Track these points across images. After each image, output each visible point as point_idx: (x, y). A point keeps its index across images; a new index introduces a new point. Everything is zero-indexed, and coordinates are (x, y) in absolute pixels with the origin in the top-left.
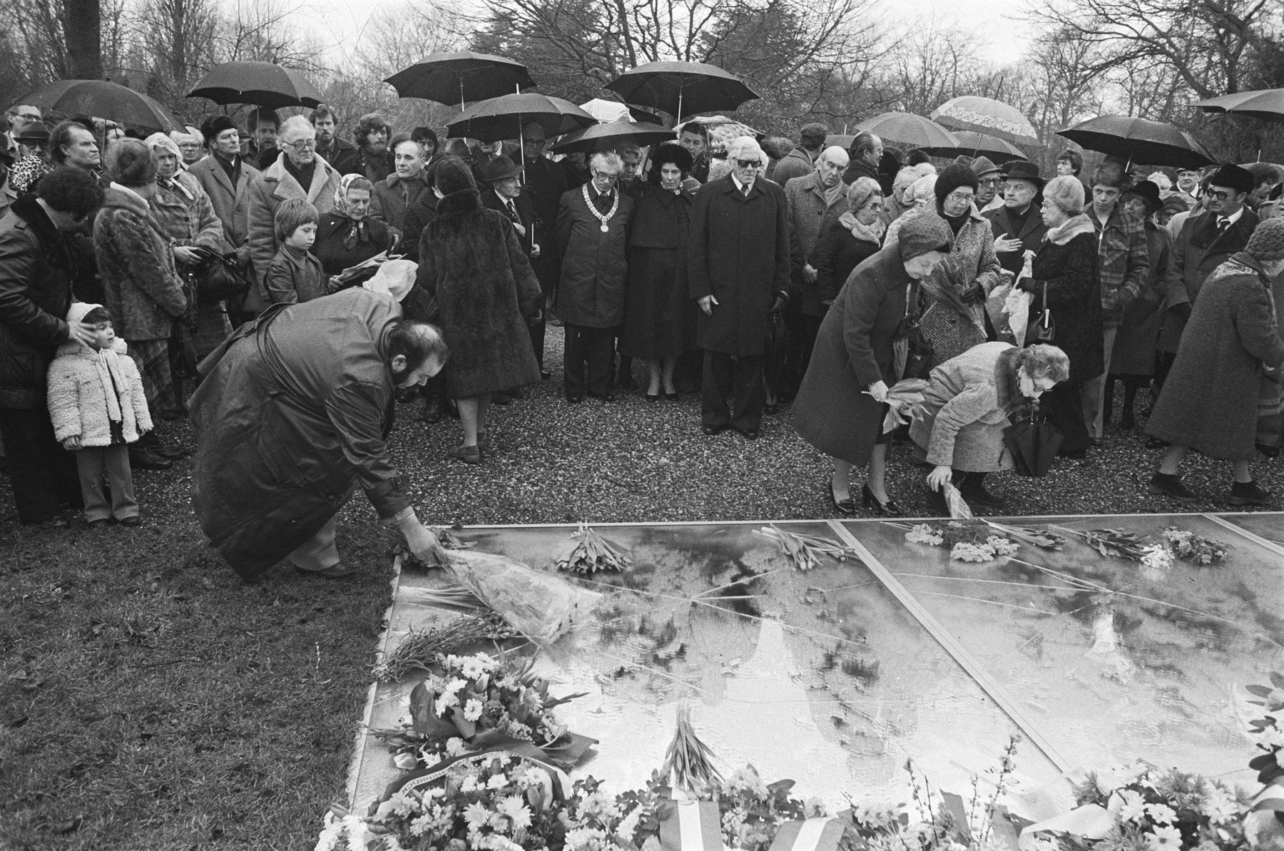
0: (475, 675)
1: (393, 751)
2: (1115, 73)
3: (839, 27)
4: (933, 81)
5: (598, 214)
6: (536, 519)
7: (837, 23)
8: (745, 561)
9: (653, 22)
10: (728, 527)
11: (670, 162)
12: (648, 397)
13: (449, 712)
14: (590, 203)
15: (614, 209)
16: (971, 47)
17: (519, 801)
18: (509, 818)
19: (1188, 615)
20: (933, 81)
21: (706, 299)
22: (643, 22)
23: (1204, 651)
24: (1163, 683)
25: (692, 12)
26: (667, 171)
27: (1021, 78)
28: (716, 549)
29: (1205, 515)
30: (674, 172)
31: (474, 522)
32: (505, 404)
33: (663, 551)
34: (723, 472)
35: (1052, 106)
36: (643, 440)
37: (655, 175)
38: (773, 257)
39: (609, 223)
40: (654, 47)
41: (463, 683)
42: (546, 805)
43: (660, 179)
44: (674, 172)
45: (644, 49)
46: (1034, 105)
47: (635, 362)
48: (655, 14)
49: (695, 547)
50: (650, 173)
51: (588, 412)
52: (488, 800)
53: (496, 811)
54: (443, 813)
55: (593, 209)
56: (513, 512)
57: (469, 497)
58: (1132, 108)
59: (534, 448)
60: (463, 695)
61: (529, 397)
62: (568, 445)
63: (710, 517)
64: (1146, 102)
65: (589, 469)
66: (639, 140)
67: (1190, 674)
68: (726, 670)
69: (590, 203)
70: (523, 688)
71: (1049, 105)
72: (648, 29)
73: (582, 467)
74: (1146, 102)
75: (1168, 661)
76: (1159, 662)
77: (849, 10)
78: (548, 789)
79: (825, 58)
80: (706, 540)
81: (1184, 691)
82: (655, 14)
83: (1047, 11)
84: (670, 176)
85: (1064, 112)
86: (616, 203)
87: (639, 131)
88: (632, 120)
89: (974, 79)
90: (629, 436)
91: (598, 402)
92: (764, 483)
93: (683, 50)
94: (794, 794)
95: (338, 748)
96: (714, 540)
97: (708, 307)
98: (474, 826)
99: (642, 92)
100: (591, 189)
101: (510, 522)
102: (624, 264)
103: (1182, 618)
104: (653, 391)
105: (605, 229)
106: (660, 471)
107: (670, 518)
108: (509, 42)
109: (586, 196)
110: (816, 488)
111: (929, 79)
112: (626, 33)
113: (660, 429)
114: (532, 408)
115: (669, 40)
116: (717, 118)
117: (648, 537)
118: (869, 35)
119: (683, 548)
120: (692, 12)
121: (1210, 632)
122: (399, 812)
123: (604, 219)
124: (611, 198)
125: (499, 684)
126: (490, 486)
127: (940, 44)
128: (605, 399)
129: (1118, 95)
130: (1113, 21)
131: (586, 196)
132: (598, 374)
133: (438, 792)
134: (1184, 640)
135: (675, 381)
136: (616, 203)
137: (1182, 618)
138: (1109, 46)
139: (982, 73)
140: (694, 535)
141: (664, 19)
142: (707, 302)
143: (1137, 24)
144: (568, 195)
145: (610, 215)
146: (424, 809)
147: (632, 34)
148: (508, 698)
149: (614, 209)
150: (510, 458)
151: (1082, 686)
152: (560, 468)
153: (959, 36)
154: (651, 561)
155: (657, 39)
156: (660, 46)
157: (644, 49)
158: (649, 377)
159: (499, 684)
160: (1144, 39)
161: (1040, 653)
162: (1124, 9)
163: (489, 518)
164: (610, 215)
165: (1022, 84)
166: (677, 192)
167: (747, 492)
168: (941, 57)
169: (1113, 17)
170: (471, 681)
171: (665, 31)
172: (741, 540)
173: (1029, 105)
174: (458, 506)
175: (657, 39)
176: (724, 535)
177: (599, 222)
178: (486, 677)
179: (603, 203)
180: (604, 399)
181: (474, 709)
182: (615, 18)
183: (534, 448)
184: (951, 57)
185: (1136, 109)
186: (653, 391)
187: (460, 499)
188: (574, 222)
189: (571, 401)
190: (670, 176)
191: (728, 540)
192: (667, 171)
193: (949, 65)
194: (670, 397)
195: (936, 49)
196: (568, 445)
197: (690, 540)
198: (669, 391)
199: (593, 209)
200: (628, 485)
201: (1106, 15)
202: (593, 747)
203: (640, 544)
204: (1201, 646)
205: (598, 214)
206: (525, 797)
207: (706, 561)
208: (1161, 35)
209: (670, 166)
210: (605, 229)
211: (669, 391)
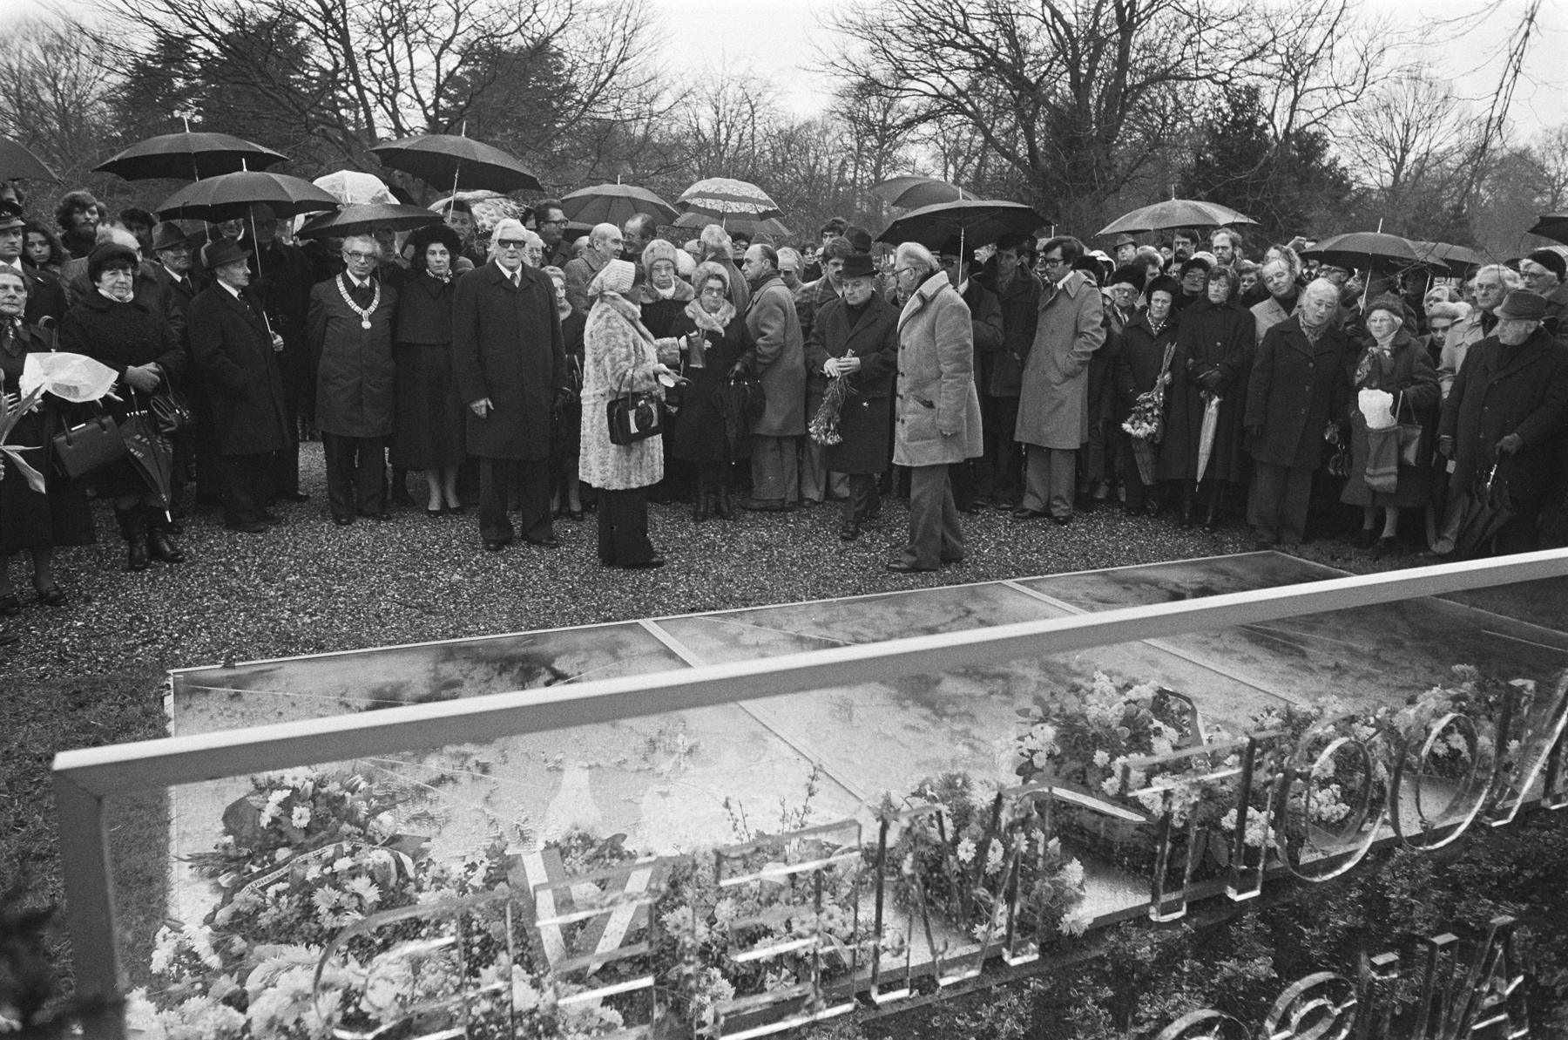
0: (298, 784)
1: (213, 875)
2: (926, 129)
3: (615, 78)
4: (728, 135)
5: (357, 309)
6: (321, 648)
7: (611, 74)
8: (557, 666)
9: (389, 70)
10: (534, 636)
11: (437, 241)
12: (429, 513)
13: (275, 820)
14: (347, 297)
15: (376, 302)
16: (768, 96)
17: (365, 880)
18: (359, 896)
19: (983, 670)
20: (728, 135)
21: (483, 402)
22: (378, 69)
23: (994, 697)
24: (958, 727)
25: (438, 58)
26: (434, 253)
27: (827, 131)
28: (526, 658)
29: (1005, 582)
30: (442, 253)
31: (248, 658)
32: (260, 531)
33: (468, 665)
34: (523, 584)
35: (863, 164)
36: (430, 558)
37: (420, 261)
38: (549, 348)
39: (370, 318)
40: (392, 99)
41: (287, 793)
42: (392, 882)
43: (425, 264)
44: (442, 253)
45: (381, 102)
46: (844, 162)
47: (410, 475)
48: (391, 60)
49: (502, 659)
50: (413, 259)
51: (361, 532)
52: (334, 880)
53: (345, 892)
54: (290, 903)
55: (351, 303)
56: (292, 645)
57: (237, 634)
58: (946, 171)
59: (305, 575)
60: (286, 805)
61: (287, 523)
62: (344, 570)
63: (515, 629)
64: (960, 160)
65: (372, 593)
66: (398, 224)
67: (982, 719)
68: (550, 764)
69: (347, 297)
70: (348, 794)
71: (859, 162)
72: (384, 79)
73: (364, 591)
74: (960, 160)
75: (962, 709)
76: (955, 710)
77: (624, 60)
78: (393, 869)
79: (605, 112)
80: (513, 651)
81: (976, 732)
82: (391, 60)
83: (844, 64)
84: (439, 257)
85: (876, 171)
86: (377, 296)
87: (400, 216)
88: (394, 201)
89: (776, 133)
90: (414, 556)
91: (370, 522)
92: (568, 592)
93: (429, 103)
94: (627, 846)
95: (150, 880)
96: (523, 651)
97: (484, 411)
98: (323, 909)
99: (392, 163)
100: (347, 281)
101: (291, 654)
102: (393, 364)
103: (977, 673)
104: (434, 506)
105: (366, 325)
106: (455, 590)
107: (470, 634)
108: (185, 78)
109: (342, 288)
110: (624, 592)
111: (724, 131)
112: (357, 83)
113: (448, 545)
114: (295, 534)
115: (410, 91)
116: (480, 193)
117: (449, 654)
118: (653, 88)
119: (489, 661)
120: (438, 58)
121: (1000, 681)
122: (243, 908)
123: (365, 314)
124: (372, 289)
125: (324, 790)
126: (260, 620)
127: (733, 92)
128: (379, 519)
129: (930, 152)
130: (912, 78)
131: (342, 288)
132: (362, 494)
133: (282, 886)
134: (979, 691)
135: (459, 494)
136: (377, 296)
137: (977, 673)
138: (910, 103)
139: (783, 125)
140: (502, 647)
141: (403, 66)
142: (481, 406)
143: (939, 82)
144: (319, 288)
145: (372, 309)
146: (268, 902)
147: (363, 82)
148: (335, 802)
149: (376, 302)
150: (278, 589)
151: (886, 738)
152: (339, 595)
153: (754, 83)
154: (457, 676)
155: (397, 90)
156: (402, 98)
157: (381, 102)
158: (429, 490)
159: (324, 790)
160: (946, 97)
161: (850, 716)
162: (922, 65)
163: (266, 653)
164: (372, 309)
165: (828, 138)
166: (447, 280)
167: (552, 602)
168: (736, 107)
169: (912, 73)
170: (295, 789)
171: (405, 81)
172: (550, 647)
173: (838, 163)
174: (225, 645)
175: (397, 90)
176: (531, 644)
177: (360, 318)
178: (310, 785)
179: (363, 296)
180: (378, 519)
181: (301, 816)
182: (342, 64)
183: (307, 575)
184: (747, 107)
185: (951, 168)
186: (434, 506)
187: (226, 637)
188: (328, 318)
189: (339, 523)
190: (439, 257)
191: (535, 649)
192: (434, 253)
193: (746, 116)
194: (455, 511)
195: (730, 98)
196: (344, 570)
197: (495, 652)
198: (453, 504)
199: (351, 303)
200: (421, 606)
201: (904, 70)
202: (425, 845)
203: (443, 661)
204: (992, 693)
205: (357, 309)
206: (372, 877)
207: (516, 671)
208: (960, 93)
209: (437, 247)
210: (366, 325)
211: (453, 504)
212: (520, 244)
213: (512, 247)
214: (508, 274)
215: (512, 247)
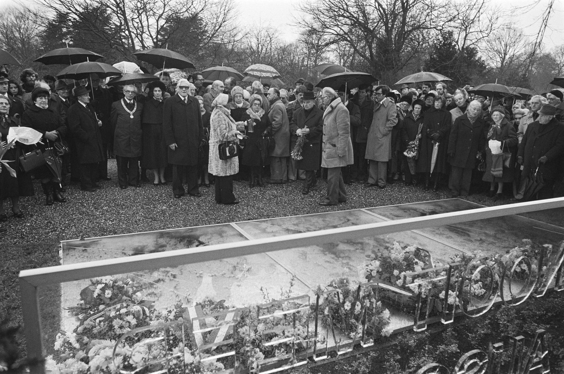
0: (107, 282)
1: (77, 315)
2: (333, 46)
3: (221, 28)
4: (262, 49)
5: (128, 111)
6: (115, 233)
7: (220, 27)
8: (200, 239)
9: (140, 25)
10: (192, 229)
11: (157, 87)
12: (154, 184)
13: (99, 295)
14: (125, 107)
15: (135, 109)
16: (276, 35)
17: (131, 317)
18: (129, 322)
19: (354, 241)
20: (262, 49)
21: (174, 145)
22: (136, 25)
23: (358, 251)
24: (345, 261)
25: (157, 21)
26: (156, 91)
27: (297, 47)
28: (189, 237)
29: (362, 209)
30: (159, 91)
31: (89, 237)
32: (93, 191)
33: (168, 239)
34: (188, 210)
35: (310, 59)
36: (155, 201)
37: (151, 94)
38: (198, 125)
39: (133, 114)
40: (141, 36)
41: (103, 285)
42: (141, 317)
43: (153, 95)
44: (159, 91)
45: (137, 37)
46: (303, 58)
47: (147, 171)
48: (141, 21)
49: (180, 237)
50: (149, 93)
51: (130, 191)
52: (120, 317)
53: (124, 321)
54: (104, 325)
55: (126, 109)
56: (105, 232)
57: (85, 228)
58: (340, 61)
59: (110, 207)
60: (103, 290)
61: (103, 188)
62: (124, 205)
63: (185, 226)
64: (345, 58)
65: (134, 213)
66: (143, 81)
67: (353, 258)
68: (198, 275)
69: (125, 107)
70: (125, 286)
71: (309, 58)
72: (138, 28)
73: (131, 213)
74: (345, 58)
75: (346, 255)
76: (343, 255)
77: (224, 21)
78: (141, 312)
79: (218, 40)
80: (184, 234)
81: (351, 263)
82: (141, 21)
83: (304, 23)
84: (158, 92)
85: (315, 61)
86: (136, 106)
87: (144, 78)
88: (142, 72)
89: (279, 48)
90: (149, 200)
91: (133, 188)
92: (204, 213)
93: (154, 37)
94: (226, 304)
95: (54, 317)
96: (188, 234)
97: (174, 148)
98: (116, 327)
99: (141, 59)
100: (125, 101)
101: (105, 235)
102: (141, 131)
103: (351, 242)
104: (156, 182)
105: (132, 117)
106: (164, 212)
107: (169, 228)
109: (123, 104)
110: (224, 213)
111: (260, 47)
112: (128, 30)
113: (161, 196)
114: (106, 192)
115: (148, 33)
116: (173, 69)
117: (162, 235)
118: (235, 32)
119: (176, 238)
120: (157, 21)
121: (360, 245)
122: (88, 327)
123: (131, 113)
124: (134, 104)
125: (117, 284)
126: (93, 223)
127: (264, 33)
128: (136, 187)
129: (335, 55)
130: (328, 28)
131: (123, 104)
132: (130, 178)
133: (101, 319)
134: (352, 249)
135: (165, 178)
136: (136, 106)
137: (351, 242)
138: (327, 37)
139: (282, 45)
140: (181, 233)
141: (145, 24)
142: (173, 146)
143: (338, 29)
144: (115, 104)
145: (134, 111)
146: (97, 324)
147: (131, 29)
148: (120, 288)
149: (135, 109)
150: (100, 212)
151: (319, 265)
152: (122, 214)
153: (271, 30)
154: (164, 243)
155: (143, 32)
156: (144, 35)
157: (137, 37)
158: (154, 176)
159: (117, 284)
160: (340, 35)
161: (306, 257)
162: (332, 23)
163: (96, 235)
164: (134, 111)
165: (298, 50)
166: (161, 101)
167: (198, 216)
168: (265, 39)
169: (328, 26)
170: (106, 284)
171: (146, 29)
172: (198, 233)
173: (301, 58)
174: (81, 232)
175: (143, 32)
176: (191, 232)
177: (129, 114)
178: (111, 282)
179: (130, 107)
180: (136, 187)
181: (108, 293)
182: (123, 23)
183: (110, 207)
184: (269, 38)
185: (342, 60)
186: (156, 182)
187: (81, 229)
188: (118, 114)
189: (122, 188)
190: (158, 92)
191: (192, 233)
192: (156, 91)
193: (268, 42)
194: (164, 184)
195: (263, 35)
196: (124, 205)
197: (178, 234)
198: (163, 181)
199: (126, 109)
200: (151, 218)
201: (325, 25)
202: (153, 304)
203: (159, 238)
204: (357, 249)
205: (128, 111)
206: (134, 315)
207: (186, 241)
208: (345, 33)
209: (157, 89)
210: (132, 117)
211: (163, 181)
212: (187, 88)
213: (184, 89)
215: (184, 89)
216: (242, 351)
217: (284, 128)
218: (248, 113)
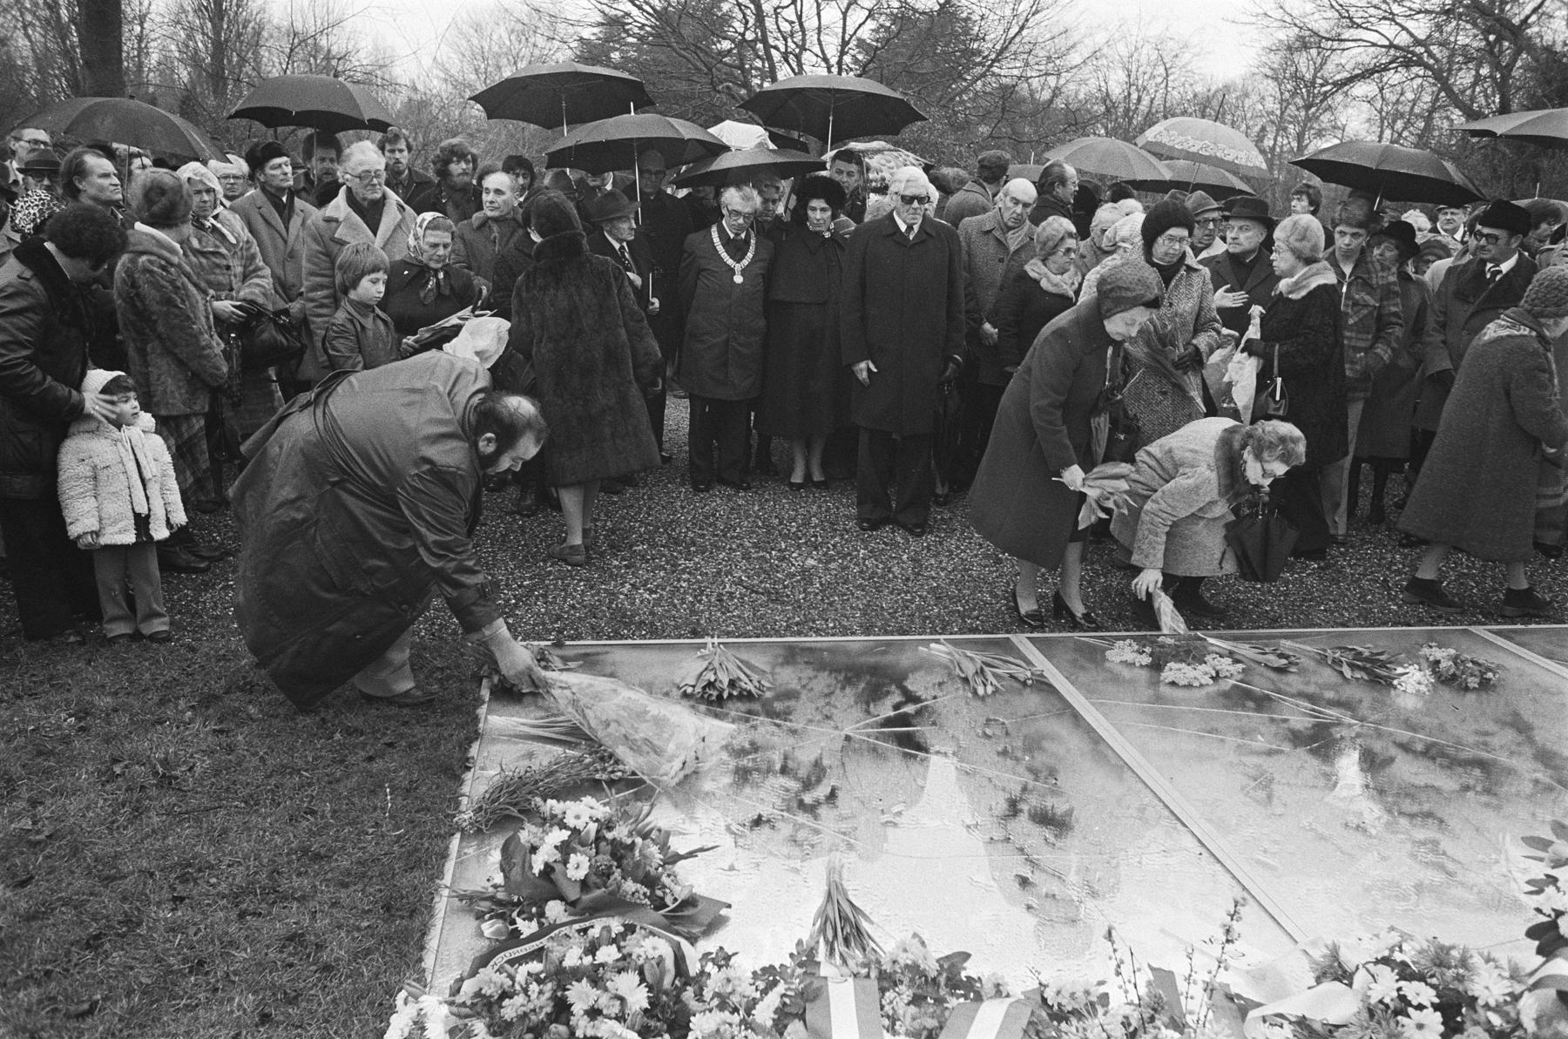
0: (580, 824)
1: (480, 917)
2: (1362, 89)
3: (1025, 32)
4: (1139, 99)
5: (730, 262)
6: (654, 633)
7: (1022, 28)
8: (910, 685)
9: (797, 27)
10: (889, 644)
11: (818, 197)
12: (792, 485)
13: (548, 869)
14: (720, 248)
15: (750, 255)
16: (1186, 57)
17: (634, 978)
18: (622, 999)
19: (1451, 751)
20: (1139, 99)
21: (863, 365)
22: (785, 27)
23: (1470, 794)
24: (1421, 834)
25: (845, 14)
26: (814, 209)
27: (1247, 95)
28: (874, 670)
29: (1472, 628)
30: (823, 210)
31: (579, 637)
32: (617, 493)
33: (810, 672)
34: (883, 577)
35: (1285, 129)
36: (785, 537)
37: (800, 214)
38: (944, 313)
39: (743, 273)
40: (798, 58)
41: (565, 834)
42: (667, 983)
43: (807, 218)
44: (823, 210)
45: (786, 60)
46: (1263, 129)
47: (775, 441)
48: (800, 17)
49: (849, 668)
50: (794, 211)
51: (718, 502)
52: (596, 977)
53: (606, 990)
54: (541, 992)
55: (725, 256)
56: (627, 625)
57: (573, 607)
58: (1382, 132)
59: (652, 546)
60: (565, 849)
61: (646, 485)
62: (694, 544)
63: (867, 631)
64: (1399, 125)
65: (719, 572)
66: (781, 170)
67: (1453, 823)
68: (886, 818)
69: (720, 248)
70: (639, 840)
71: (1281, 129)
72: (792, 36)
73: (711, 570)
74: (1399, 125)
75: (1426, 807)
76: (1415, 809)
77: (1037, 12)
78: (669, 963)
79: (1008, 70)
80: (862, 659)
81: (1446, 844)
82: (800, 17)
83: (1278, 14)
84: (818, 215)
85: (1300, 137)
86: (752, 248)
87: (780, 160)
88: (772, 146)
89: (1190, 96)
90: (769, 532)
91: (730, 491)
92: (933, 590)
93: (834, 61)
94: (970, 970)
95: (413, 913)
96: (872, 660)
97: (865, 375)
98: (578, 1009)
99: (784, 112)
100: (721, 231)
101: (623, 637)
102: (762, 323)
103: (1444, 755)
104: (797, 478)
105: (738, 279)
106: (806, 575)
107: (818, 632)
109: (716, 240)
110: (996, 596)
111: (1134, 96)
112: (764, 41)
113: (806, 524)
114: (650, 498)
115: (817, 49)
116: (876, 144)
117: (791, 655)
118: (1061, 43)
119: (834, 670)
120: (845, 14)
121: (1477, 772)
122: (487, 991)
123: (738, 267)
124: (747, 242)
125: (609, 836)
126: (598, 593)
127: (1148, 54)
128: (738, 488)
129: (1365, 116)
130: (1359, 26)
131: (716, 240)
132: (731, 457)
133: (535, 966)
134: (1446, 782)
135: (824, 465)
136: (752, 248)
137: (1444, 755)
138: (1354, 56)
139: (1199, 89)
140: (847, 653)
141: (811, 23)
142: (863, 368)
143: (1389, 30)
144: (694, 238)
145: (745, 262)
146: (518, 987)
147: (771, 41)
148: (620, 852)
149: (750, 255)
150: (623, 559)
151: (1322, 838)
152: (683, 571)
153: (1171, 44)
154: (795, 685)
155: (803, 48)
156: (806, 56)
157: (786, 60)
158: (793, 460)
159: (609, 836)
160: (1397, 47)
161: (1270, 797)
162: (1372, 11)
163: (597, 633)
164: (745, 262)
165: (1248, 102)
166: (827, 235)
167: (912, 601)
168: (1149, 70)
169: (1359, 21)
170: (575, 831)
171: (812, 37)
172: (905, 660)
173: (1257, 129)
174: (559, 618)
175: (803, 48)
176: (884, 653)
177: (732, 271)
178: (593, 827)
179: (737, 248)
180: (738, 487)
181: (579, 866)
182: (751, 21)
183: (652, 546)
184: (1161, 70)
185: (1388, 133)
186: (797, 478)
187: (561, 609)
188: (701, 271)
189: (697, 490)
190: (818, 215)
191: (888, 659)
192: (814, 209)
193: (1159, 80)
194: (818, 485)
195: (1144, 59)
196: (694, 544)
197: (843, 659)
198: (817, 477)
199: (725, 256)
200: (767, 592)
201: (1350, 18)
202: (724, 912)
203: (782, 665)
204: (1467, 788)
205: (730, 262)
206: (641, 973)
207: (862, 685)
208: (1418, 42)
209: (818, 203)
210: (738, 279)
211: (817, 477)
212: (922, 200)
213: (916, 204)
214: (903, 228)
215: (916, 204)
216: (1074, 551)
217: (586, 36)
218: (1033, 275)
